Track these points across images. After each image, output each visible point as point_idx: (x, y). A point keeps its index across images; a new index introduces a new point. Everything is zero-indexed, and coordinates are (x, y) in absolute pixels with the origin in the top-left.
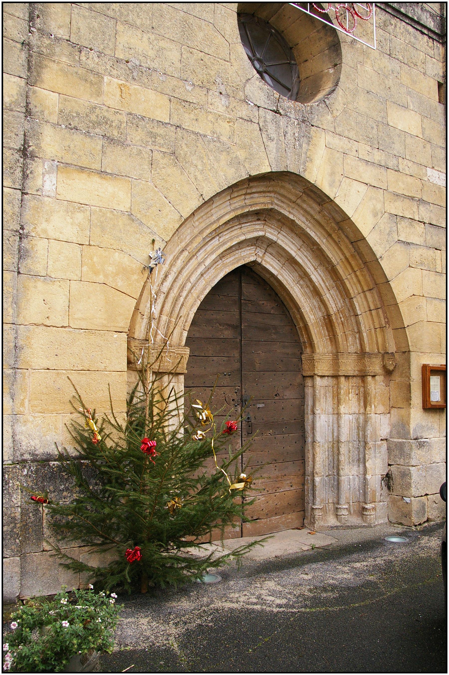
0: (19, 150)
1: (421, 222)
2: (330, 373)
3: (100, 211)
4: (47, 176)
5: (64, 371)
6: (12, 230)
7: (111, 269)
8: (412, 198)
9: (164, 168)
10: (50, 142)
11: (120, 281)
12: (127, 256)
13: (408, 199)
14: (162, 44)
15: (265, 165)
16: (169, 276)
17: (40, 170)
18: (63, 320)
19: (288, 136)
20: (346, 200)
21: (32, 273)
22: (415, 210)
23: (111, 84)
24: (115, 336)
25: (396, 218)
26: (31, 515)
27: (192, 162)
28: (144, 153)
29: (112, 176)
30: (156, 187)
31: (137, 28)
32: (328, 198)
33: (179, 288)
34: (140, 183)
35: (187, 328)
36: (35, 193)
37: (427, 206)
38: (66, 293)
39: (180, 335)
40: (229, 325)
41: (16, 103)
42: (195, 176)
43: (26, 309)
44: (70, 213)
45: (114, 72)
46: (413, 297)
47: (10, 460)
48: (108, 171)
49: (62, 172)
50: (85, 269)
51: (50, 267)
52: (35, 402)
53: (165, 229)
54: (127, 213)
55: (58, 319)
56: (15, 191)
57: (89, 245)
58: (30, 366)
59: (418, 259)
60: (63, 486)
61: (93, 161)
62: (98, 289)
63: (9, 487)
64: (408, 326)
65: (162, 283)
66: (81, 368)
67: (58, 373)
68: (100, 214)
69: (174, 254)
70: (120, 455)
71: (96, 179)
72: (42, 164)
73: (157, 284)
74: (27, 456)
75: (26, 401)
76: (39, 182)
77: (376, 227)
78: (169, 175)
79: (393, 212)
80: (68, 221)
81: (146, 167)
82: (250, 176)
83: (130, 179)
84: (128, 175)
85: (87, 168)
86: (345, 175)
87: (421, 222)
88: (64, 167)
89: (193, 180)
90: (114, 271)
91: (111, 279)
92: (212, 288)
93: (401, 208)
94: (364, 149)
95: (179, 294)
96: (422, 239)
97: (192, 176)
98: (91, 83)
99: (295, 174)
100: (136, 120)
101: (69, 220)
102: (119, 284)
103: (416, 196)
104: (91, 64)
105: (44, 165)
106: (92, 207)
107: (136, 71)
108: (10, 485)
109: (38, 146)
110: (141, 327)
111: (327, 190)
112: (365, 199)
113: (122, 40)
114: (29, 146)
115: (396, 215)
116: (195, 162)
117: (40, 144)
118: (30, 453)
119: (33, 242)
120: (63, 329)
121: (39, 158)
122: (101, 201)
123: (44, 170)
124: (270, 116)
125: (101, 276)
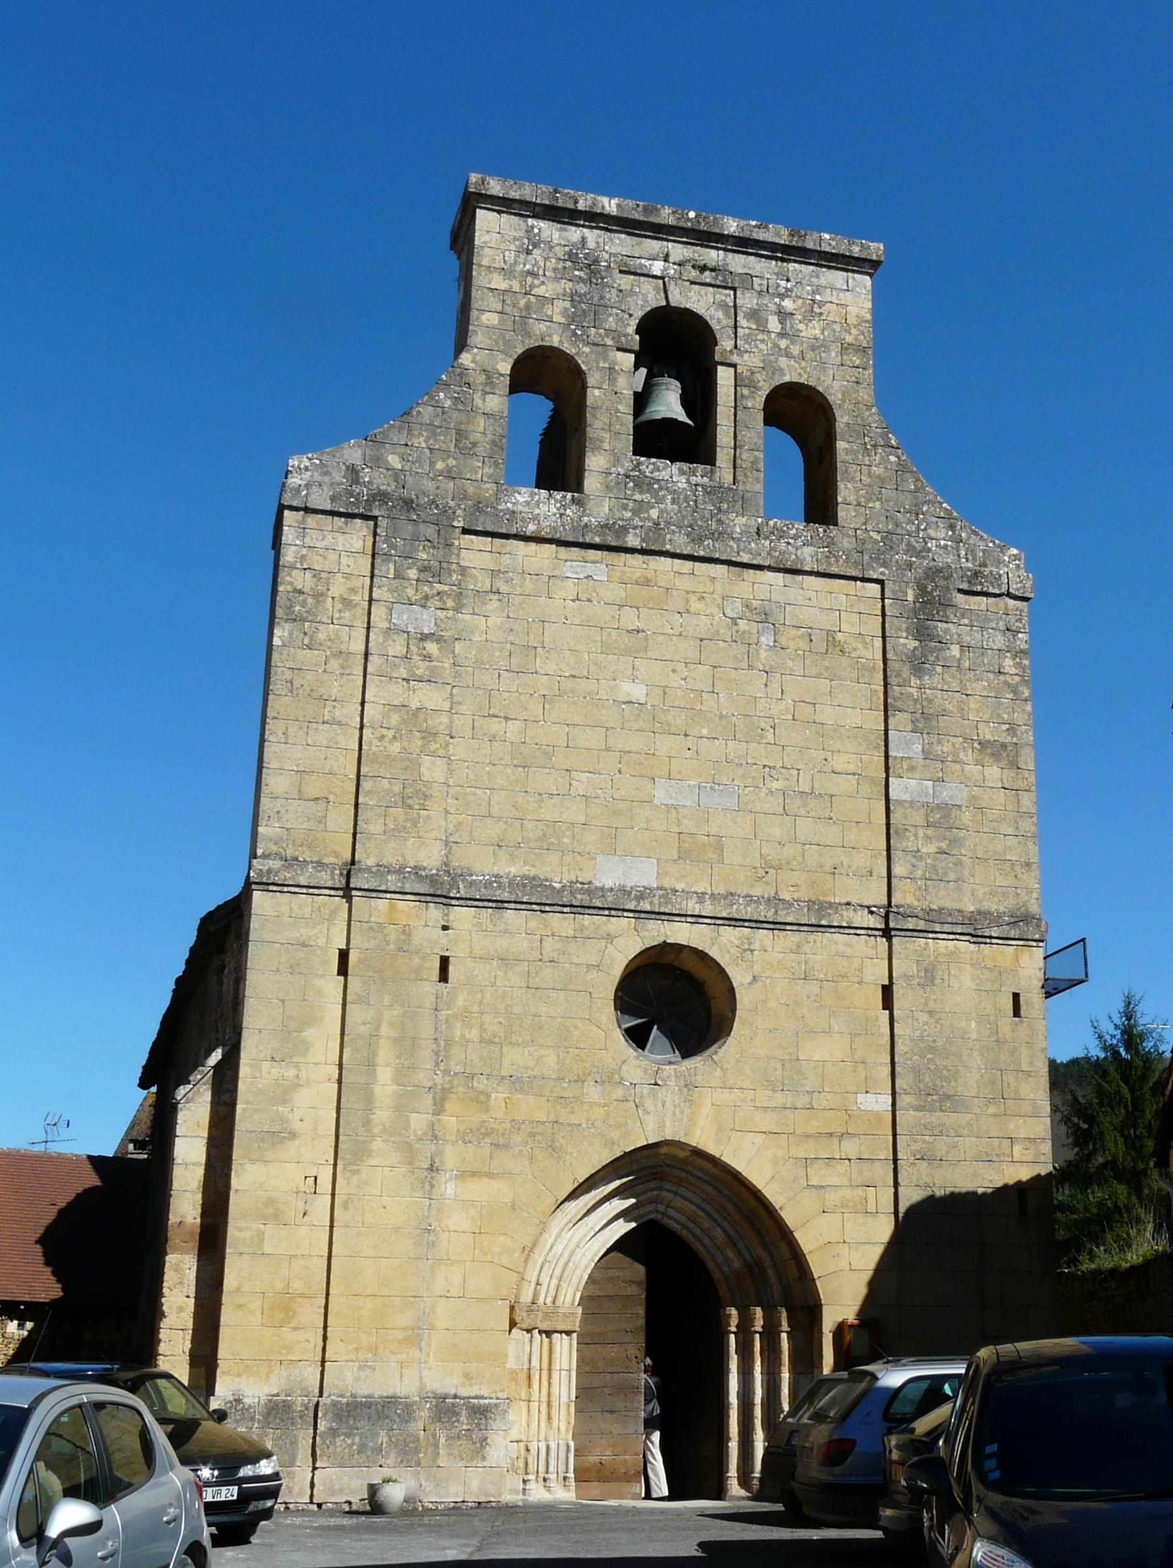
2: (368, 858)
8: (831, 1134)
10: (451, 1157)
14: (542, 1052)
19: (668, 1105)
23: (498, 1098)
31: (519, 1045)
37: (856, 1139)
39: (571, 1295)
41: (425, 1134)
45: (500, 1089)
53: (543, 1212)
55: (455, 1292)
71: (485, 1179)
74: (430, 1395)
76: (443, 1188)
79: (802, 1155)
88: (464, 1175)
94: (763, 1097)
98: (482, 1102)
101: (464, 1214)
104: (481, 1087)
107: (517, 1083)
109: (442, 1161)
111: (712, 1150)
113: (507, 1060)
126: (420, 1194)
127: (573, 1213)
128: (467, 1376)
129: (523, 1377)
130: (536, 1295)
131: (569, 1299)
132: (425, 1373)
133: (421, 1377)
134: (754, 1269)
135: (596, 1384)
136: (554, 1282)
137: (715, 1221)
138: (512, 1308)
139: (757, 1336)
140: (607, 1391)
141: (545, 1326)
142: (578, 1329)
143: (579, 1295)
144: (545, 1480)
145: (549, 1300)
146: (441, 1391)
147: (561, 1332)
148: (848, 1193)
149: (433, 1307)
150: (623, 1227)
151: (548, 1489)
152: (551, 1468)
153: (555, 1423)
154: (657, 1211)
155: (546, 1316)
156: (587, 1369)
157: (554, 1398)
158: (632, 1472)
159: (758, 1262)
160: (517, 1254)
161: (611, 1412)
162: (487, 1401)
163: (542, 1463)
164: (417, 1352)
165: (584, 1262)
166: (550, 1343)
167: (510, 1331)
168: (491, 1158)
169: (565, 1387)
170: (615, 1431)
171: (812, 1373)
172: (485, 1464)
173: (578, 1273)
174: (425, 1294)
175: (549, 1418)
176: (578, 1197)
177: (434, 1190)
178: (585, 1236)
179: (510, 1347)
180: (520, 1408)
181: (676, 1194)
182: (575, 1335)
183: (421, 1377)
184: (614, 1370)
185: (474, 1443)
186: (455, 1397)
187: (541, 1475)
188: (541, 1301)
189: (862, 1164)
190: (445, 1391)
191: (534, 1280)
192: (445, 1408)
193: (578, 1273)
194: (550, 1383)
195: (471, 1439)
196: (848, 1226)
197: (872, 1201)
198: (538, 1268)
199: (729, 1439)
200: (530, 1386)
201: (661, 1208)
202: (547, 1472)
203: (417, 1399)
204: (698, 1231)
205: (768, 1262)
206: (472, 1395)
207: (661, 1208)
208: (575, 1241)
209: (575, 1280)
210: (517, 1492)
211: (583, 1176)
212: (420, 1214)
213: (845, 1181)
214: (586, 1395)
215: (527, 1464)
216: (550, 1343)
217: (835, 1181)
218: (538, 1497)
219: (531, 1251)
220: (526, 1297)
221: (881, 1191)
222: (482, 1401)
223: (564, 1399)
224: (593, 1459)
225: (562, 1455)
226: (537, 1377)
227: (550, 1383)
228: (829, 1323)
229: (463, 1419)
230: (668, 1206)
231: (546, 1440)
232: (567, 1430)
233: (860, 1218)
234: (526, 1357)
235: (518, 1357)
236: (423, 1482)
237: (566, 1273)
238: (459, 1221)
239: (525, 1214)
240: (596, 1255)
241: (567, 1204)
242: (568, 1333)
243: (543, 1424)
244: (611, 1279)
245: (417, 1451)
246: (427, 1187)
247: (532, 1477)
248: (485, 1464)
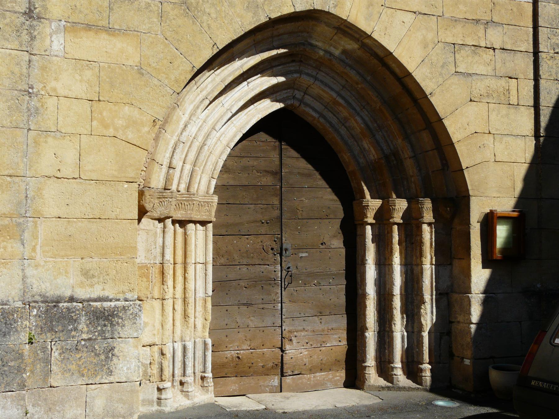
0: (25, 13)
1: (488, 48)
3: (109, 67)
4: (54, 37)
5: (75, 220)
6: (20, 90)
7: (120, 122)
8: (478, 21)
9: (174, 19)
11: (130, 133)
12: (137, 109)
13: (471, 23)
15: (288, 5)
16: (189, 126)
17: (48, 31)
18: (74, 172)
20: (387, 33)
21: (43, 129)
22: (480, 35)
24: (126, 186)
26: (39, 352)
27: (204, 10)
28: (152, 5)
29: (120, 32)
30: (166, 39)
32: (365, 33)
33: (204, 137)
34: (150, 36)
35: (216, 176)
36: (43, 53)
37: (500, 29)
38: (76, 147)
39: (205, 183)
40: (266, 171)
42: (208, 24)
43: (37, 162)
44: (78, 71)
46: (475, 135)
47: (20, 301)
48: (116, 27)
49: (69, 32)
50: (95, 123)
51: (60, 123)
52: (47, 248)
53: (177, 81)
54: (136, 68)
55: (67, 171)
56: (22, 52)
57: (99, 100)
58: (42, 215)
59: (483, 92)
60: (72, 326)
61: (100, 18)
62: (108, 142)
63: (18, 325)
64: (467, 168)
65: (181, 134)
66: (92, 216)
67: (69, 222)
68: (110, 70)
69: (194, 103)
71: (104, 36)
72: (49, 25)
73: (176, 134)
74: (37, 298)
75: (38, 247)
77: (426, 60)
78: (180, 26)
79: (450, 40)
80: (77, 78)
81: (155, 20)
82: (270, 18)
83: (139, 33)
84: (136, 29)
85: (94, 26)
86: (387, 5)
87: (488, 48)
89: (206, 29)
90: (124, 124)
91: (121, 132)
92: (244, 135)
93: (461, 35)
95: (203, 143)
96: (490, 69)
97: (204, 25)
99: (324, 11)
101: (78, 77)
102: (129, 137)
103: (483, 18)
105: (51, 26)
106: (101, 64)
108: (19, 323)
110: (159, 176)
111: (363, 25)
112: (412, 30)
114: (35, 8)
115: (454, 44)
116: (207, 10)
117: (46, 5)
118: (40, 295)
119: (43, 100)
120: (74, 180)
121: (46, 19)
122: (109, 57)
123: (51, 30)
125: (111, 130)
126: (15, 45)
127: (209, 89)
128: (86, 274)
129: (155, 272)
130: (168, 179)
131: (203, 188)
132: (30, 272)
133: (24, 277)
134: (392, 161)
135: (232, 276)
136: (188, 167)
137: (354, 109)
138: (141, 194)
139: (395, 228)
140: (242, 283)
141: (179, 215)
142: (214, 219)
143: (214, 182)
144: (182, 384)
145: (182, 187)
146: (51, 292)
147: (195, 222)
148: (494, 83)
149: (39, 189)
150: (267, 107)
151: (186, 394)
152: (189, 371)
153: (191, 320)
154: (294, 97)
155: (180, 205)
156: (222, 259)
157: (190, 295)
158: (271, 364)
159: (396, 154)
160: (146, 129)
161: (248, 305)
162: (113, 304)
163: (178, 365)
164: (17, 246)
165: (219, 148)
166: (185, 234)
167: (139, 220)
168: (111, 9)
169: (201, 282)
170: (252, 325)
171: (451, 264)
172: (112, 379)
173: (213, 158)
174: (28, 173)
175: (185, 316)
176: (221, 65)
177: (36, 43)
178: (222, 117)
179: (139, 239)
180: (153, 307)
181: (316, 79)
182: (210, 226)
183: (24, 277)
184: (251, 262)
185: (97, 355)
186: (72, 299)
187: (178, 378)
188: (174, 187)
189: (505, 55)
190: (58, 293)
191: (166, 163)
192: (56, 314)
193: (213, 158)
194: (185, 278)
195: (93, 350)
196: (493, 117)
197: (514, 92)
198: (170, 149)
199: (365, 328)
200: (163, 282)
201: (299, 95)
202: (184, 374)
203: (19, 304)
204: (334, 120)
205: (406, 153)
206: (94, 295)
207: (299, 95)
208: (210, 122)
209: (210, 166)
210: (150, 403)
211: (223, 41)
212: (16, 70)
213: (491, 73)
214: (223, 287)
215: (162, 370)
216: (185, 234)
217: (481, 69)
218: (176, 405)
219: (162, 127)
220: (157, 181)
221: (522, 83)
222: (106, 304)
223: (200, 294)
224: (230, 354)
225: (199, 353)
226: (171, 272)
227: (185, 278)
228: (477, 212)
229: (82, 326)
230: (305, 93)
231: (182, 340)
232: (204, 327)
233: (504, 109)
234: (159, 250)
235: (148, 251)
236: (30, 409)
237: (202, 157)
238: (70, 82)
239: (156, 82)
240: (231, 140)
241: (206, 74)
242: (203, 223)
243: (178, 323)
244: (245, 169)
245: (20, 370)
246: (25, 37)
247: (168, 384)
248: (112, 379)
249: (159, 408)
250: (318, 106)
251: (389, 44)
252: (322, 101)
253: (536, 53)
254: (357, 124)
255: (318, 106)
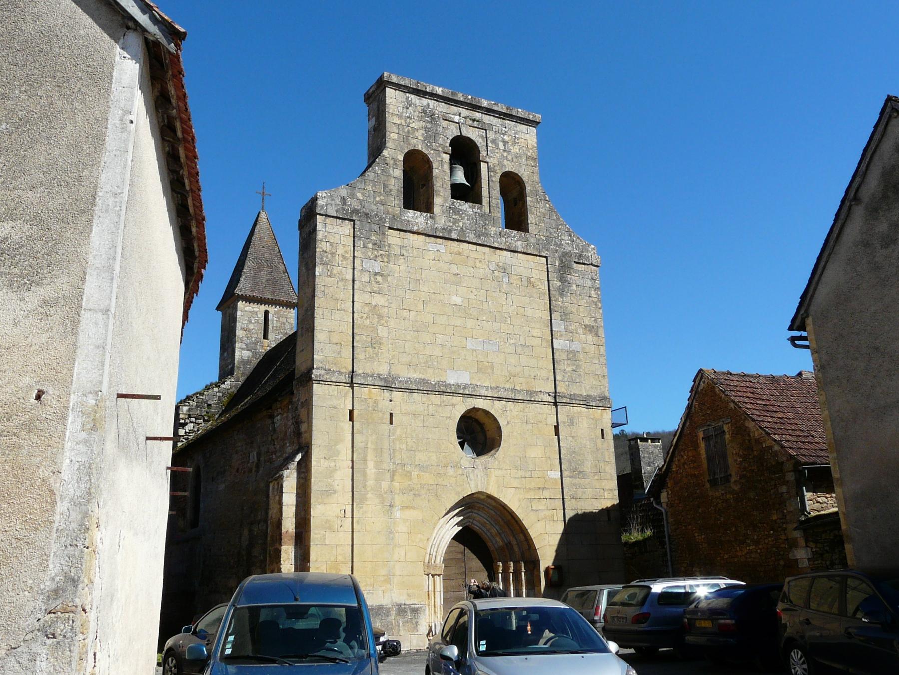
2: (358, 370)
10: (398, 500)
25: (531, 500)
39: (440, 559)
70: (726, 600)
88: (404, 508)
100: (422, 486)
107: (422, 468)
111: (496, 495)
124: (471, 470)
128: (409, 595)
134: (509, 545)
148: (546, 512)
156: (446, 590)
159: (510, 543)
189: (552, 501)
196: (548, 526)
205: (514, 542)
228: (542, 569)
238: (402, 528)
242: (439, 575)
249: (863, 205)
250: (479, 524)
251: (506, 501)
252: (481, 523)
253: (563, 499)
254: (494, 531)
255: (479, 524)
